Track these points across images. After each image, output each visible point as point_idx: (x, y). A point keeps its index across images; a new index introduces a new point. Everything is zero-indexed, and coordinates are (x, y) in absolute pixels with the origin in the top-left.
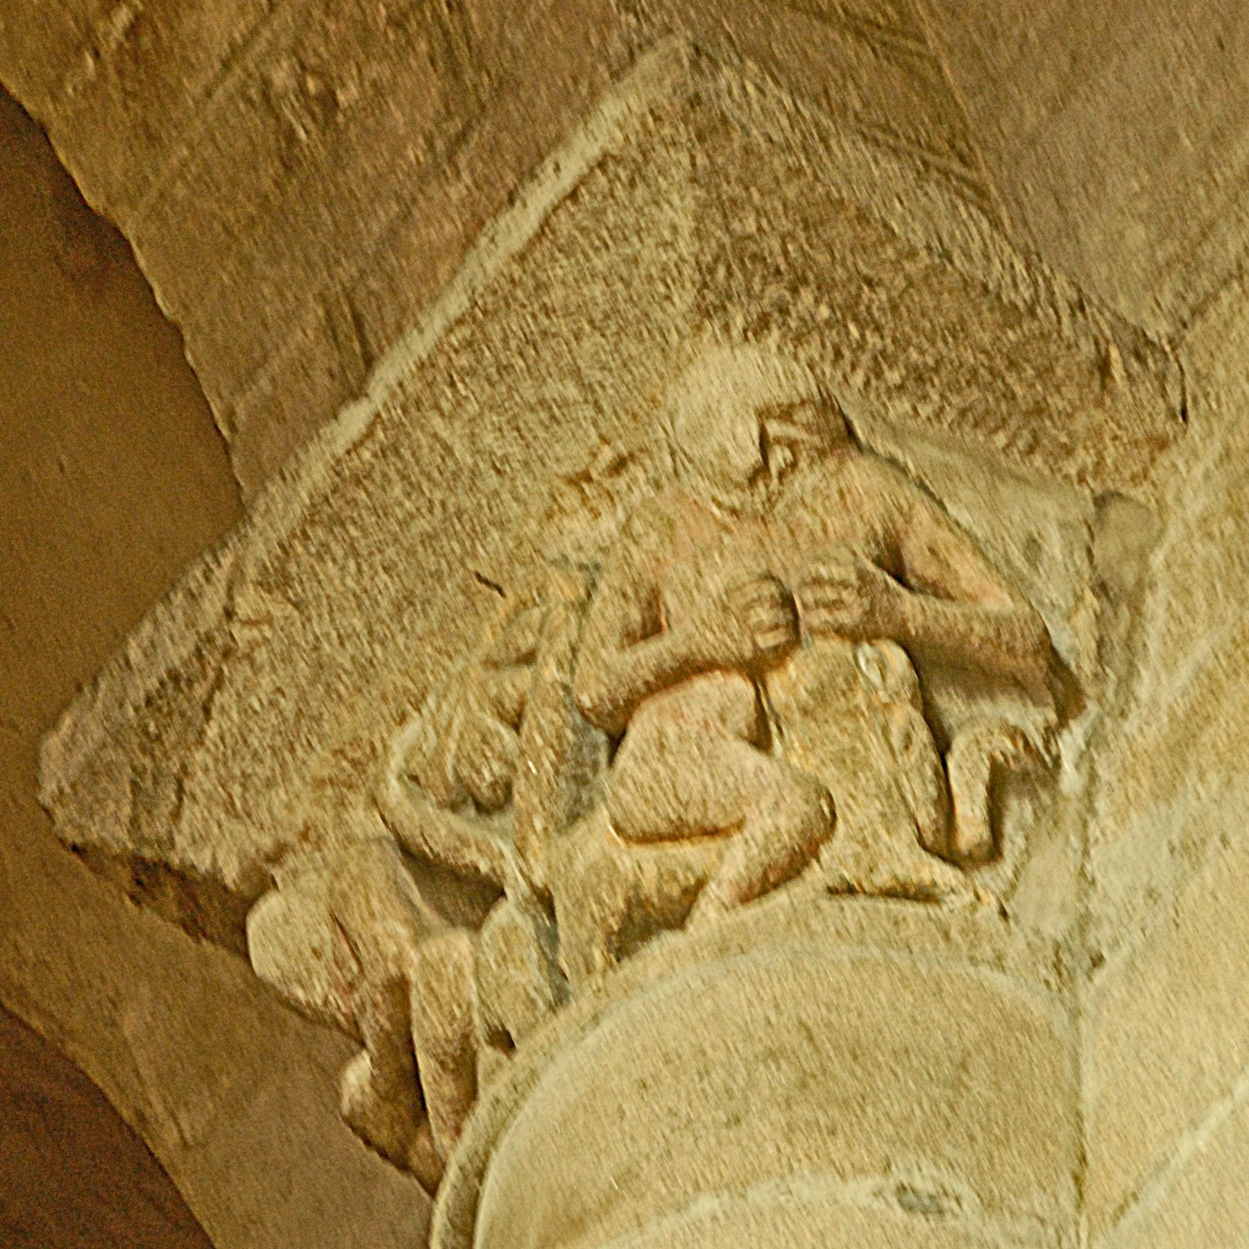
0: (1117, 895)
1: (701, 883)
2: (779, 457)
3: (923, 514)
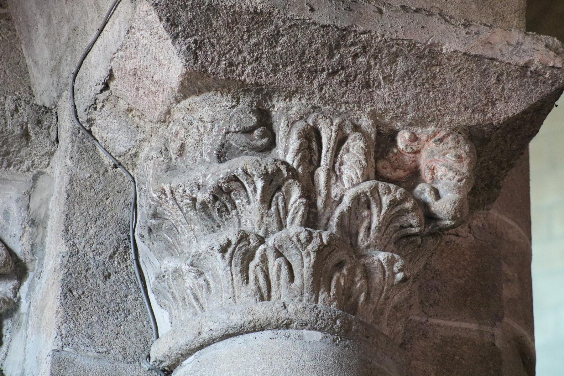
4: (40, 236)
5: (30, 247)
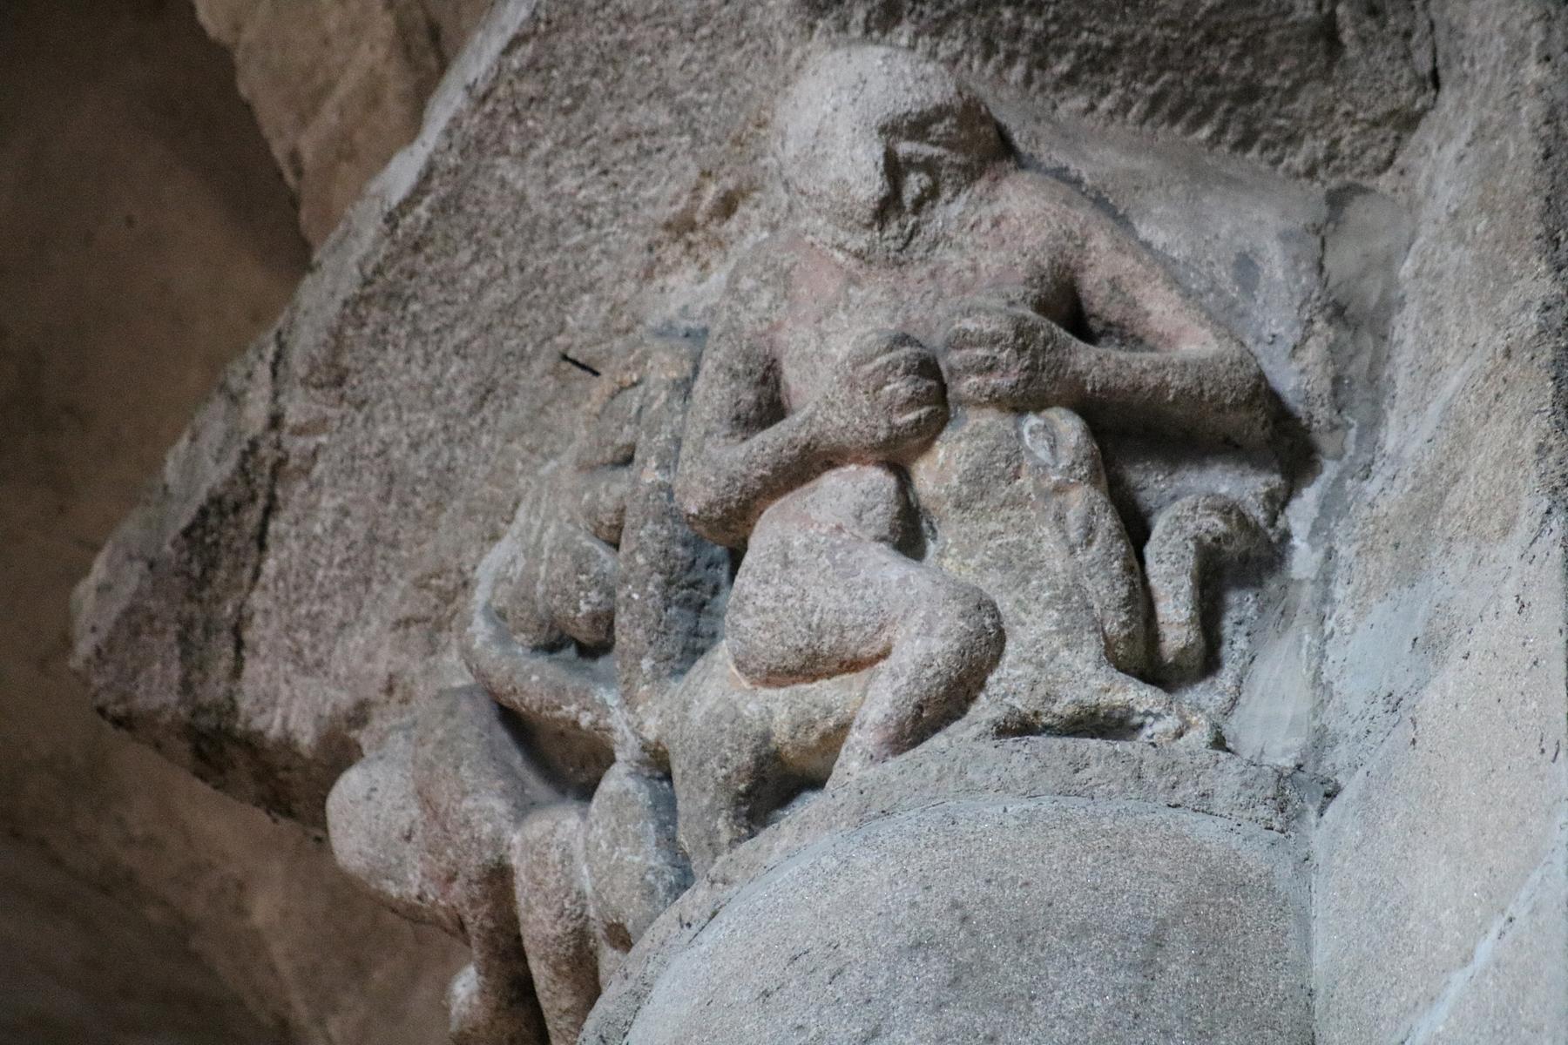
0: (1357, 707)
1: (843, 728)
2: (914, 184)
3: (1101, 241)
4: (1365, 359)
5: (1326, 384)
